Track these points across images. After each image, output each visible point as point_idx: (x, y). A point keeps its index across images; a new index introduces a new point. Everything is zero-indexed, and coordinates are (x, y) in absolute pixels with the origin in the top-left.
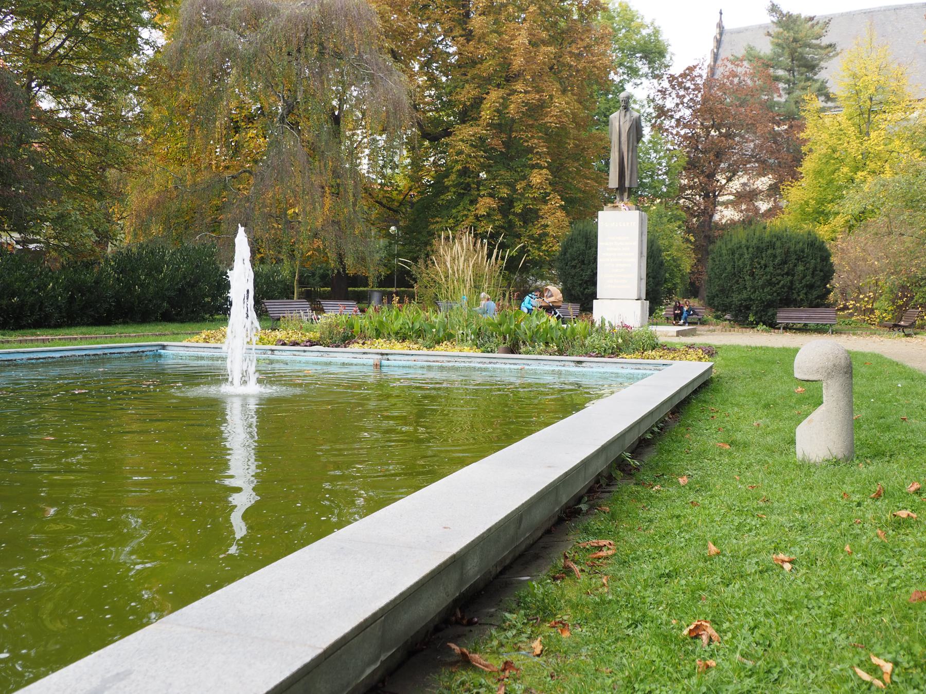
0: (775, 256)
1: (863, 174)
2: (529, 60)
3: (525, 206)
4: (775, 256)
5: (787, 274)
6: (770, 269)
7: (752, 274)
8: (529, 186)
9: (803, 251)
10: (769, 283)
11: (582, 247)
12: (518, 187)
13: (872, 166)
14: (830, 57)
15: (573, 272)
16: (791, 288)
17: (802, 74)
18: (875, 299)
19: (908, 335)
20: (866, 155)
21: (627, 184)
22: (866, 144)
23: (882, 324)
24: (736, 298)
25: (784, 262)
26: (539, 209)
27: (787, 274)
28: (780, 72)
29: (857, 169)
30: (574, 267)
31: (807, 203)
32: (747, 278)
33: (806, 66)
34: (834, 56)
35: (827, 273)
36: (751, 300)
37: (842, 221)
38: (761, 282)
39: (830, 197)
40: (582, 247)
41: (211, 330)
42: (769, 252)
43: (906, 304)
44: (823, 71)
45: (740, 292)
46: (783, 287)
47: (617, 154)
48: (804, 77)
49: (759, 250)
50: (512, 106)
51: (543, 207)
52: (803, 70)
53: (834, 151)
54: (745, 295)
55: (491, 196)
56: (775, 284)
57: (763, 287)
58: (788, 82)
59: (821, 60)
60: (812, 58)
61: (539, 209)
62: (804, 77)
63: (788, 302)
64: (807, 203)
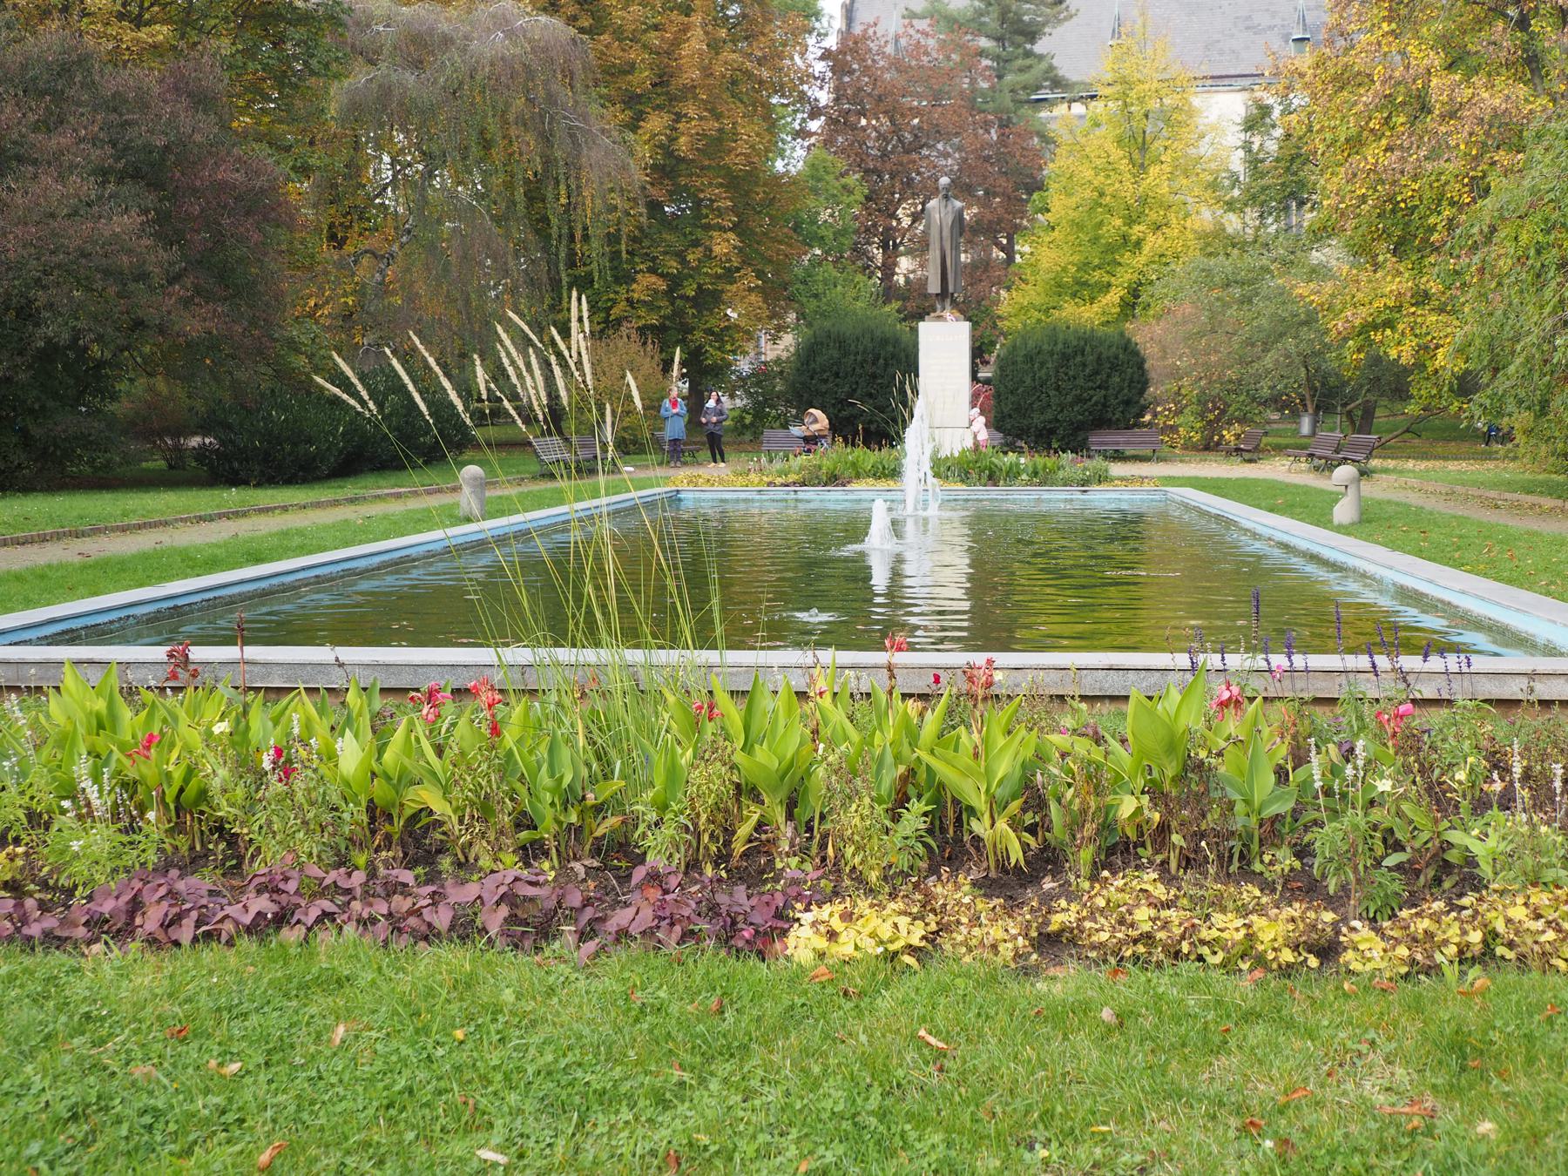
0: (1084, 365)
1: (1142, 228)
2: (707, 72)
3: (700, 286)
4: (1084, 365)
5: (1099, 387)
6: (1080, 382)
7: (1058, 388)
8: (709, 254)
9: (1116, 358)
10: (1079, 400)
11: (836, 354)
12: (690, 257)
13: (1153, 216)
14: (1060, 21)
15: (824, 388)
16: (1104, 405)
17: (1019, 46)
18: (1179, 412)
19: (1250, 461)
20: (1143, 200)
21: (951, 289)
22: (1144, 184)
23: (1189, 447)
24: (1037, 419)
25: (1097, 373)
26: (722, 291)
27: (1099, 387)
28: (984, 43)
29: (1130, 222)
30: (826, 381)
31: (1064, 269)
32: (1052, 393)
33: (1022, 33)
34: (1066, 19)
35: (1140, 381)
36: (1057, 421)
37: (1117, 299)
38: (1069, 398)
39: (1096, 261)
40: (836, 354)
41: (1021, 452)
42: (1079, 359)
43: (1218, 419)
44: (1045, 39)
45: (1042, 411)
46: (1096, 404)
47: (938, 253)
48: (1020, 51)
49: (1066, 358)
50: (682, 140)
51: (728, 287)
52: (1020, 39)
53: (1102, 195)
54: (1049, 415)
55: (652, 271)
56: (1086, 401)
57: (1072, 405)
58: (997, 58)
59: (1044, 25)
60: (1032, 22)
61: (722, 291)
62: (1020, 51)
63: (1101, 422)
64: (1064, 269)
